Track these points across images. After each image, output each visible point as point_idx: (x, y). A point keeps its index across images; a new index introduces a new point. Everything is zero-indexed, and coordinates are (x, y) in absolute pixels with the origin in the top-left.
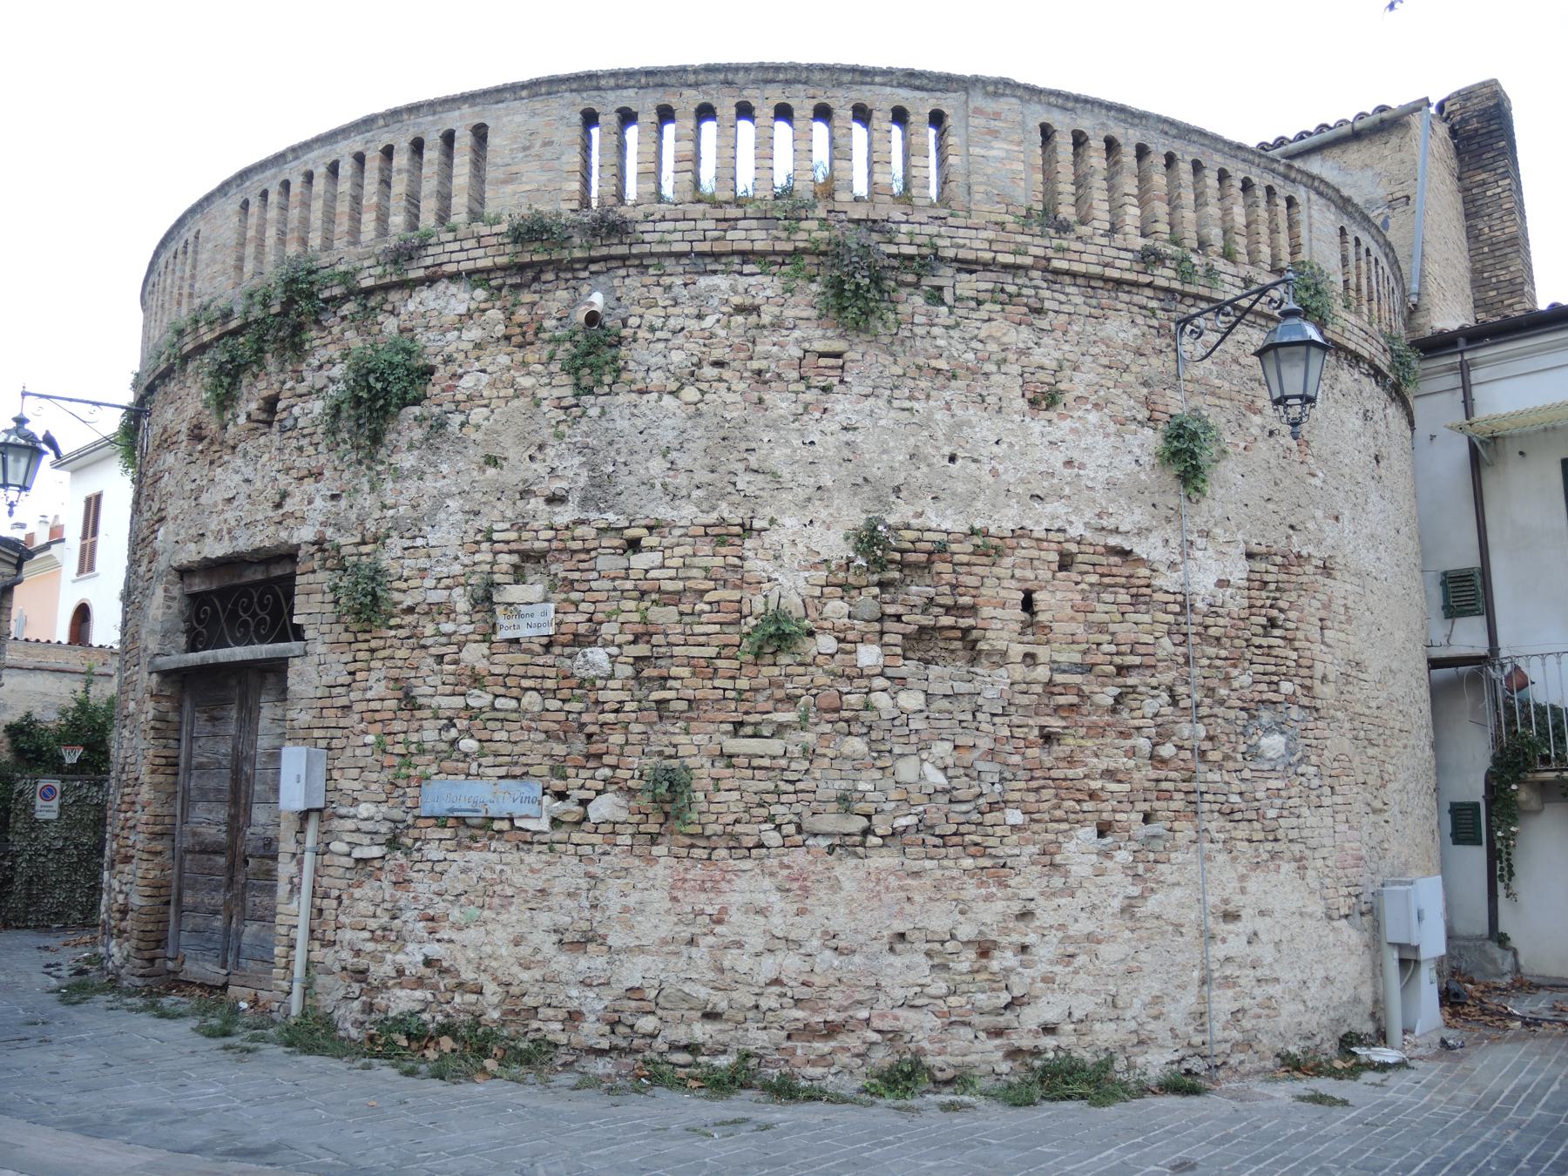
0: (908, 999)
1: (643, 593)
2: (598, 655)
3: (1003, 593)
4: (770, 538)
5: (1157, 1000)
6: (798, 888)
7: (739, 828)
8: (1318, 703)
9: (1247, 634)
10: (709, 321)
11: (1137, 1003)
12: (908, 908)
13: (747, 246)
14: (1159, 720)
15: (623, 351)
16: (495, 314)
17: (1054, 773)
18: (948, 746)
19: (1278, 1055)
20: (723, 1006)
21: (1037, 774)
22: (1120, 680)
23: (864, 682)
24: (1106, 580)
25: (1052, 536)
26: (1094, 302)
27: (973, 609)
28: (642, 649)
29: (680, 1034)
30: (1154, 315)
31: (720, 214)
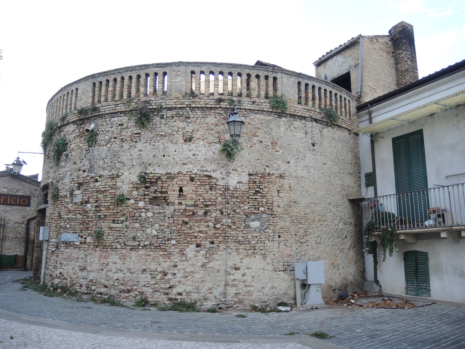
0: (145, 284)
1: (98, 191)
2: (89, 205)
3: (174, 188)
4: (122, 178)
5: (210, 289)
6: (123, 258)
7: (112, 244)
8: (275, 213)
9: (248, 195)
10: (113, 128)
11: (204, 289)
12: (146, 263)
13: (120, 110)
15: (97, 137)
16: (77, 130)
17: (184, 232)
18: (158, 225)
19: (251, 306)
20: (107, 284)
21: (180, 232)
22: (205, 208)
23: (139, 210)
25: (188, 173)
26: (204, 114)
27: (166, 192)
28: (96, 204)
29: (98, 290)
30: (222, 115)
31: (115, 103)
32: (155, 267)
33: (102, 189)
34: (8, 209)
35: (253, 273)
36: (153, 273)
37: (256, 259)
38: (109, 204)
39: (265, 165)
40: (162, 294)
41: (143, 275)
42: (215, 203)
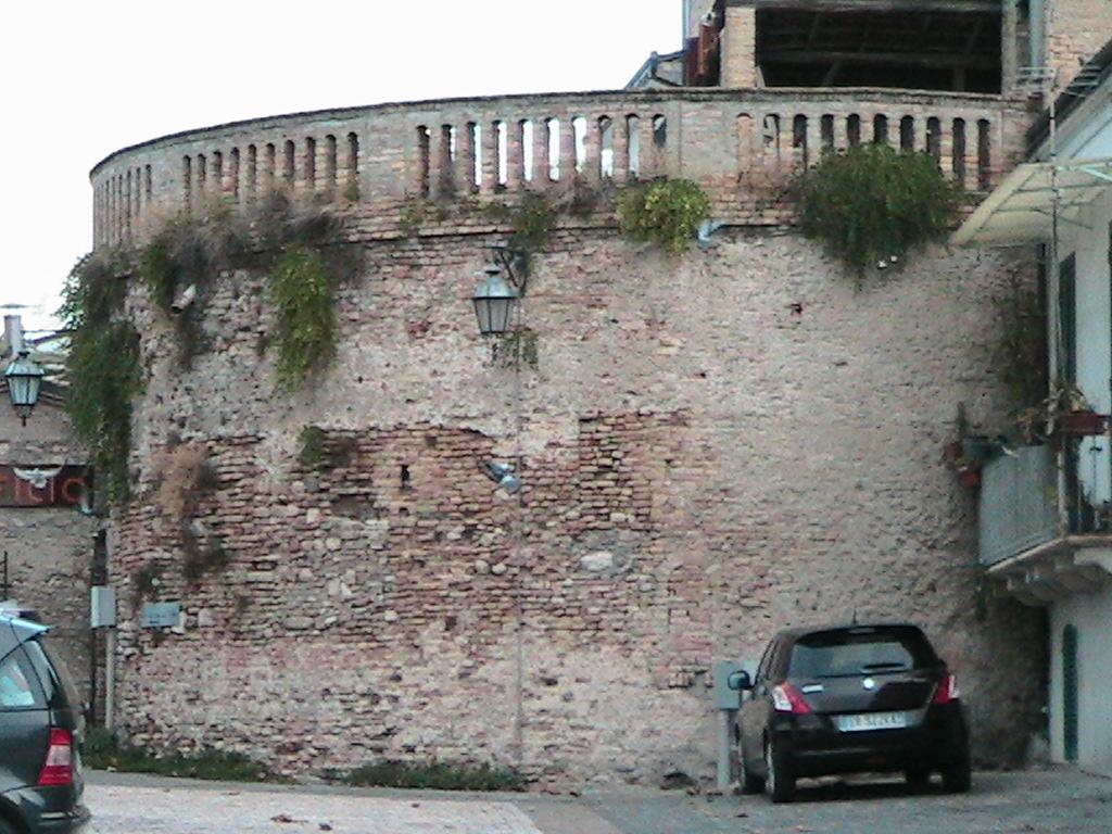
5: (481, 734)
6: (279, 662)
8: (657, 526)
9: (576, 480)
10: (241, 299)
11: (466, 735)
12: (331, 674)
14: (493, 548)
24: (457, 453)
27: (368, 482)
32: (351, 682)
34: (20, 524)
38: (240, 518)
39: (626, 389)
40: (369, 752)
41: (324, 706)
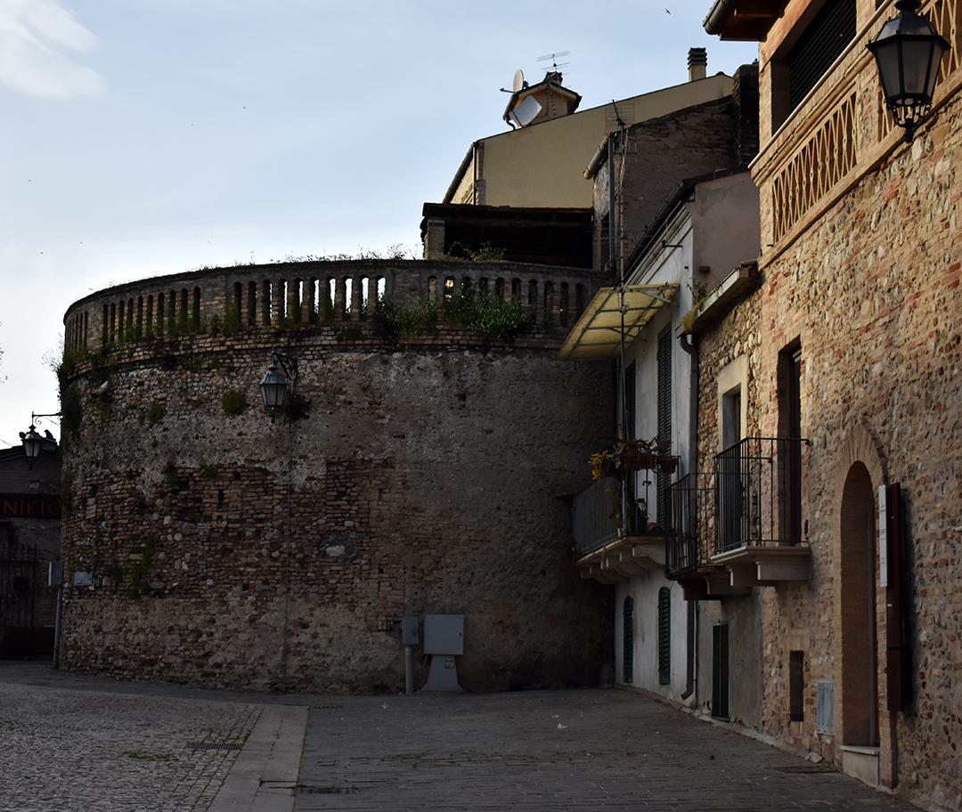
5: (262, 658)
8: (373, 530)
27: (200, 500)
32: (185, 623)
33: (118, 496)
34: (43, 527)
35: (331, 633)
36: (182, 632)
37: (337, 610)
39: (356, 444)
41: (169, 637)
42: (269, 516)
